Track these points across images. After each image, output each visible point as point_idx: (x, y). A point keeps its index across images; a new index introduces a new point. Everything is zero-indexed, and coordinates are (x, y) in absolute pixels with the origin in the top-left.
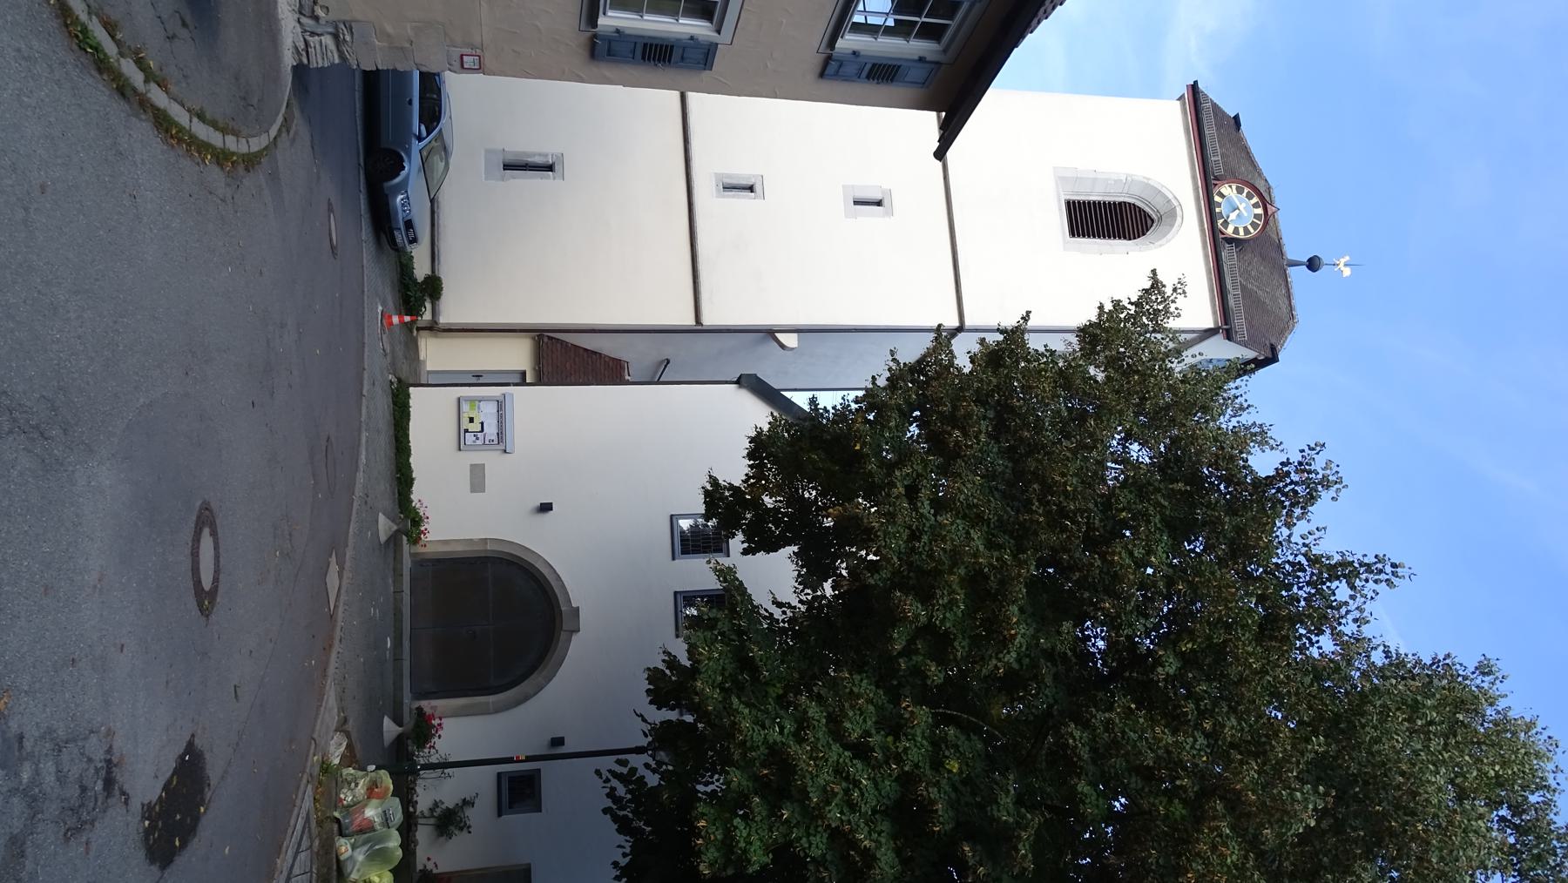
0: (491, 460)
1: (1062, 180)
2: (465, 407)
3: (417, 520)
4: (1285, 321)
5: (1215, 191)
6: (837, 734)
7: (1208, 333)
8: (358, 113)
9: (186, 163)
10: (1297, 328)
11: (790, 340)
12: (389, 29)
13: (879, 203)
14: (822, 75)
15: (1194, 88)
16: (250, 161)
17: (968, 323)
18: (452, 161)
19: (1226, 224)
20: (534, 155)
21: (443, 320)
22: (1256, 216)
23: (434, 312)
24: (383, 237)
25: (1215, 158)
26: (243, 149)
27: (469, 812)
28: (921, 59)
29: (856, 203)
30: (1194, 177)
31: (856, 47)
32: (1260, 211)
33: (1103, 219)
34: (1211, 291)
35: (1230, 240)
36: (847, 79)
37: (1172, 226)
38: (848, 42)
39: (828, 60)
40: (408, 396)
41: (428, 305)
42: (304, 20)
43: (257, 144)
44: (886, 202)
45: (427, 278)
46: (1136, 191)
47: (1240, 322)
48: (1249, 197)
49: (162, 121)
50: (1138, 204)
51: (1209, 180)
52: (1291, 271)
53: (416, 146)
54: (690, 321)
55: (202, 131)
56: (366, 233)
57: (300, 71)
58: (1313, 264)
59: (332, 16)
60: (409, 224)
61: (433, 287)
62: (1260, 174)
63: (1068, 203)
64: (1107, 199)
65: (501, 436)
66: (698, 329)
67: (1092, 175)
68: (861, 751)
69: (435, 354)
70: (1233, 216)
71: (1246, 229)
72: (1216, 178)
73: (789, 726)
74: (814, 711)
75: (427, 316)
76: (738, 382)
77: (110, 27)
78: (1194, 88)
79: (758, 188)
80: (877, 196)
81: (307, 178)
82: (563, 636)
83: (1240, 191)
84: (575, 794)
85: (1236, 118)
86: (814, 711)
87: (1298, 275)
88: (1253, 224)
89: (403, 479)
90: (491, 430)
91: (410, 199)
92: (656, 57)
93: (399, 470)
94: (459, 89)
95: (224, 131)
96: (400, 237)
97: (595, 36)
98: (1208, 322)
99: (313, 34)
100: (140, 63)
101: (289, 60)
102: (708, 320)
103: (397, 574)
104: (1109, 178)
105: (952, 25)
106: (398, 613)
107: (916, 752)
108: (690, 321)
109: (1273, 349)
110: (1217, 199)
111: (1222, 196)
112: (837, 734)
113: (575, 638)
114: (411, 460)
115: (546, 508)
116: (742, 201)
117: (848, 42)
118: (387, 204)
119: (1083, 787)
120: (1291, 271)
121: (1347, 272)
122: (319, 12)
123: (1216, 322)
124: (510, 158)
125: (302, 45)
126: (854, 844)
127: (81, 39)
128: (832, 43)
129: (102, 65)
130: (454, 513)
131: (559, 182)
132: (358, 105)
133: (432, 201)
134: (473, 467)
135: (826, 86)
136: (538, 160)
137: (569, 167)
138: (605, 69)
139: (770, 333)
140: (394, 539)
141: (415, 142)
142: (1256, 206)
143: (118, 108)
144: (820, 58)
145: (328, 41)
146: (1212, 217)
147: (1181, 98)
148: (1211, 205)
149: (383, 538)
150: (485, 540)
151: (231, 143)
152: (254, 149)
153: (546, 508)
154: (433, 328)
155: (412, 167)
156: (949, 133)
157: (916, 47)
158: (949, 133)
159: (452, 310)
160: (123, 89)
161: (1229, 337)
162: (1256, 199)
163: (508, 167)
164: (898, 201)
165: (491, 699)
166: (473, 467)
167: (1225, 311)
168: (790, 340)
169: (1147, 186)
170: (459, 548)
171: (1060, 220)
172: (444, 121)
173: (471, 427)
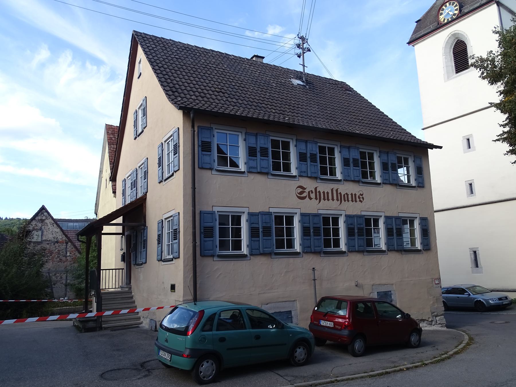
1: (449, 78)
5: (443, 23)
8: (469, 313)
9: (468, 351)
12: (432, 302)
13: (468, 140)
14: (423, 187)
15: (409, 43)
16: (471, 339)
18: (476, 285)
19: (454, 15)
20: (471, 258)
22: (450, 5)
24: (508, 307)
25: (432, 27)
26: (467, 340)
28: (414, 161)
29: (470, 148)
30: (439, 32)
31: (414, 180)
32: (448, 4)
34: (481, 10)
35: (460, 11)
36: (423, 180)
37: (458, 33)
38: (413, 183)
39: (419, 187)
42: (433, 324)
43: (466, 337)
44: (468, 138)
48: (443, 10)
49: (456, 353)
50: (453, 48)
51: (440, 26)
53: (472, 296)
55: (460, 347)
56: (504, 313)
57: (447, 327)
59: (431, 317)
60: (500, 299)
62: (435, 4)
64: (453, 59)
70: (451, 13)
71: (455, 7)
72: (438, 24)
77: (435, 358)
79: (470, 182)
80: (466, 141)
81: (480, 328)
83: (442, 14)
85: (416, 22)
88: (453, 5)
91: (492, 298)
92: (427, 232)
94: (447, 282)
95: (461, 343)
96: (505, 302)
97: (424, 250)
99: (436, 322)
100: (442, 355)
101: (445, 329)
105: (403, 156)
110: (446, 21)
111: (445, 19)
116: (475, 187)
117: (413, 183)
118: (493, 306)
122: (430, 320)
123: (494, 4)
124: (474, 265)
125: (440, 325)
127: (438, 362)
128: (414, 187)
129: (443, 360)
131: (479, 249)
132: (462, 313)
133: (491, 291)
135: (426, 185)
136: (473, 256)
137: (474, 246)
138: (433, 245)
141: (471, 296)
142: (446, 6)
143: (452, 359)
144: (418, 189)
145: (438, 318)
146: (453, 20)
148: (449, 23)
151: (465, 342)
152: (468, 338)
155: (479, 297)
156: (432, 147)
157: (411, 164)
158: (432, 147)
160: (449, 358)
162: (444, 7)
163: (477, 266)
164: (466, 134)
169: (446, 47)
172: (462, 287)
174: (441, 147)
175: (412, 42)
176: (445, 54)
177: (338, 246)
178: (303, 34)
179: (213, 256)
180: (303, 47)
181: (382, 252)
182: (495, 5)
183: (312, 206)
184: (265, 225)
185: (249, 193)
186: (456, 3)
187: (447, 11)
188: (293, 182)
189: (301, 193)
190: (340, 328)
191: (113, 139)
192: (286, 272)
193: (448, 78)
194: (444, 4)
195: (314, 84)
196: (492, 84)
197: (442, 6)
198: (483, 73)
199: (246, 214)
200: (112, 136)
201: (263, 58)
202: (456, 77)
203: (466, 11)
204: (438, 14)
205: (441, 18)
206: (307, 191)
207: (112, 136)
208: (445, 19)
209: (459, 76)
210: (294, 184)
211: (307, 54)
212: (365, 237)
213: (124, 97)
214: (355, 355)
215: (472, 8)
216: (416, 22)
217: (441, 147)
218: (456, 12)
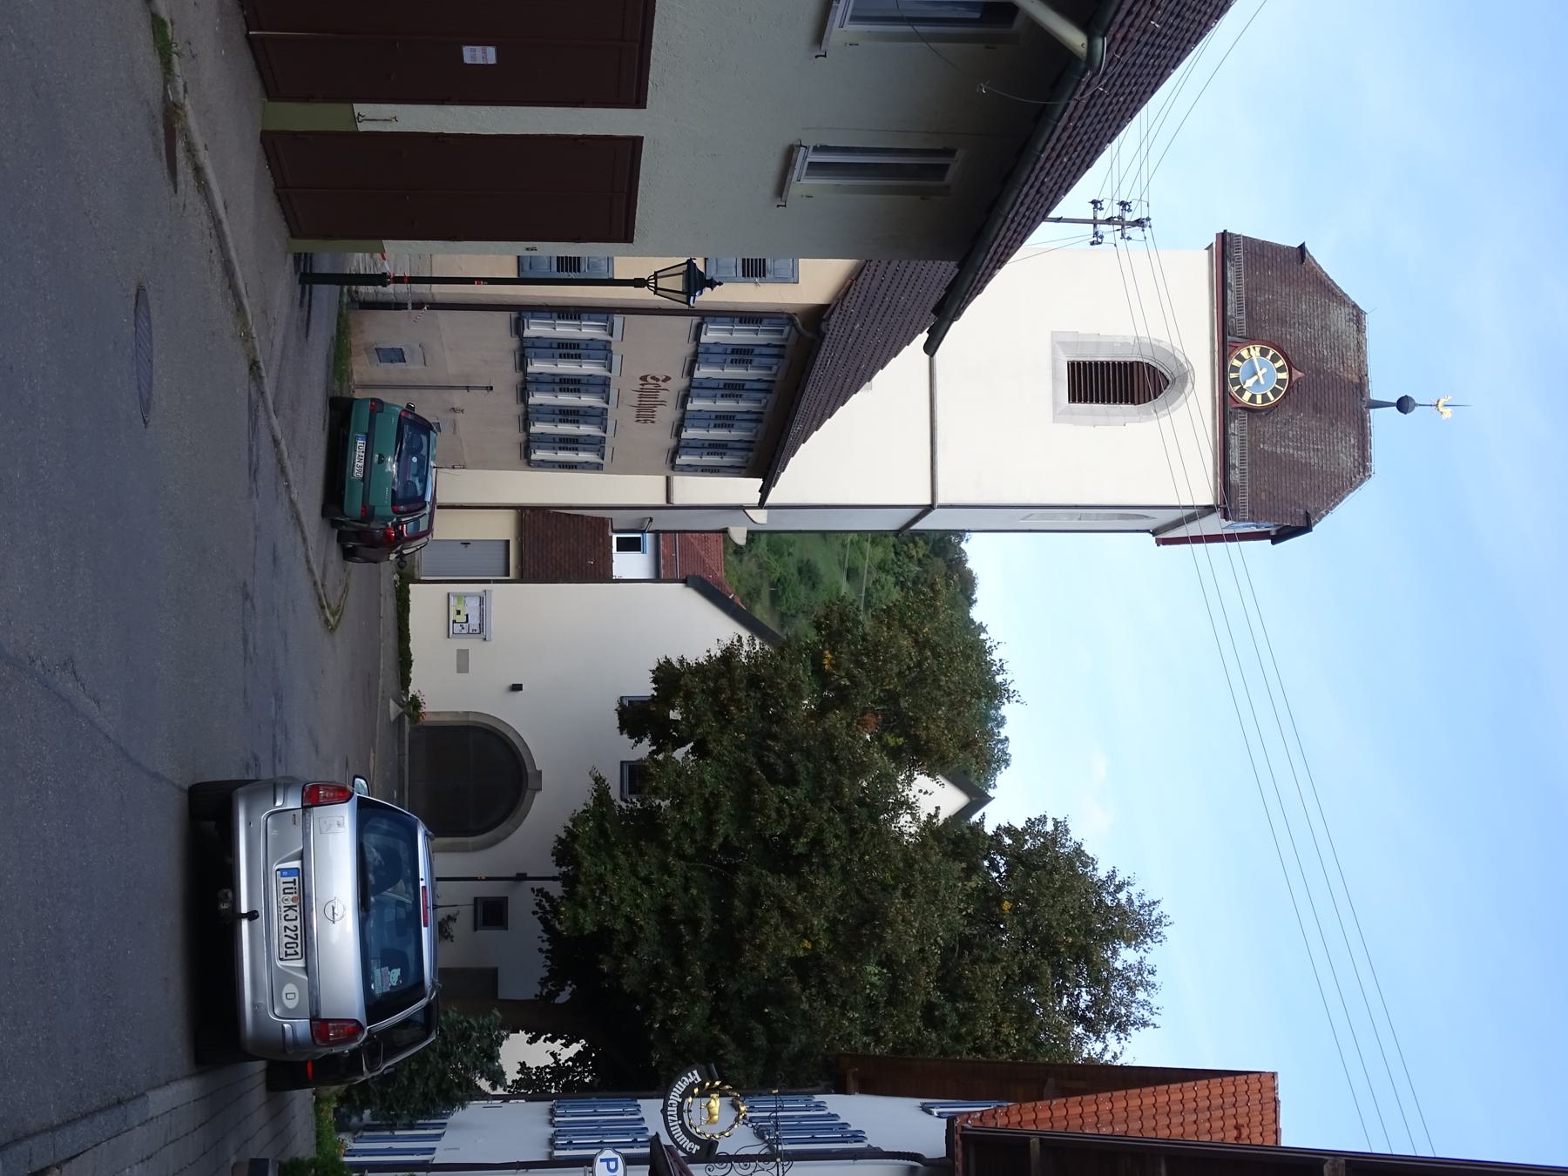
1: (1058, 342)
3: (415, 703)
6: (635, 873)
7: (1209, 510)
10: (1367, 486)
17: (941, 500)
19: (1241, 391)
27: (452, 925)
30: (1212, 339)
33: (1110, 382)
37: (1182, 391)
46: (1147, 352)
47: (1243, 500)
51: (1227, 342)
52: (1374, 413)
54: (662, 501)
58: (1404, 405)
65: (481, 625)
67: (1094, 339)
68: (647, 881)
70: (1249, 383)
73: (609, 867)
74: (622, 859)
76: (684, 581)
82: (528, 793)
83: (1264, 353)
84: (522, 904)
85: (1302, 247)
86: (622, 859)
87: (1382, 422)
89: (404, 661)
90: (474, 622)
98: (1208, 500)
102: (677, 501)
103: (401, 741)
104: (1115, 333)
106: (401, 770)
107: (674, 883)
108: (662, 501)
109: (1307, 517)
111: (1241, 359)
112: (635, 873)
113: (538, 796)
119: (737, 903)
120: (1374, 413)
126: (635, 923)
130: (440, 687)
140: (400, 718)
142: (1280, 370)
147: (1209, 248)
149: (393, 718)
150: (467, 713)
153: (517, 688)
161: (1226, 517)
165: (470, 840)
167: (1225, 485)
170: (448, 718)
173: (459, 619)
182: (1210, 502)
187: (1260, 374)
193: (1062, 344)
203: (1233, 427)
208: (1241, 359)
209: (1055, 378)
215: (1234, 441)
216: (1302, 247)
218: (1246, 397)
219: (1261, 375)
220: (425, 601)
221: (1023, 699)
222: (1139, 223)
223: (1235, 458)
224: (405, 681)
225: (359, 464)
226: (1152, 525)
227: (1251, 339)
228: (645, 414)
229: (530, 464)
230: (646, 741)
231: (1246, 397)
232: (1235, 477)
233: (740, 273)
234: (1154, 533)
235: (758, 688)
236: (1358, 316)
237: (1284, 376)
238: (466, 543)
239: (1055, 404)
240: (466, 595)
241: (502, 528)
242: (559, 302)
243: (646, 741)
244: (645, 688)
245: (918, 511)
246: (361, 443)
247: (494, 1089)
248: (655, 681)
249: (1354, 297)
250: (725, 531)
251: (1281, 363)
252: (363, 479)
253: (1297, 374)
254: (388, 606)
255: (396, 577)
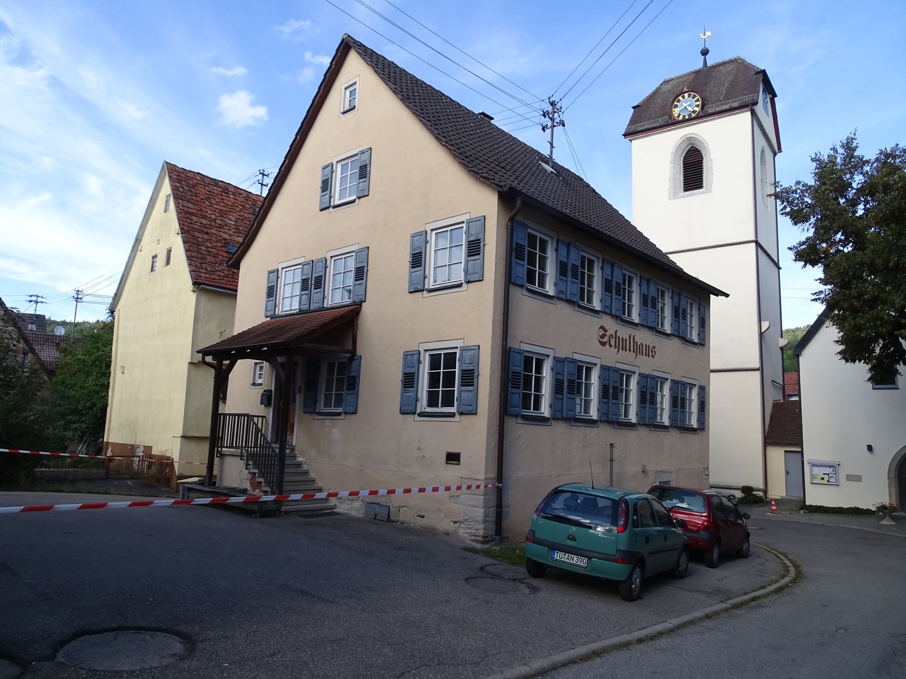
0: (842, 473)
1: (674, 196)
2: (816, 481)
3: (883, 508)
4: (739, 65)
7: (753, 114)
10: (743, 56)
11: (765, 325)
17: (753, 238)
19: (694, 112)
21: (762, 487)
22: (689, 96)
23: (759, 490)
25: (661, 122)
32: (686, 95)
33: (693, 170)
35: (703, 108)
40: (811, 506)
41: (755, 493)
45: (743, 492)
47: (747, 99)
51: (672, 123)
52: (709, 64)
58: (705, 53)
61: (747, 490)
62: (659, 89)
63: (685, 190)
65: (830, 467)
66: (761, 369)
69: (778, 491)
70: (690, 109)
75: (761, 494)
76: (798, 356)
78: (625, 135)
83: (676, 106)
85: (634, 108)
87: (711, 60)
88: (693, 98)
89: (855, 512)
90: (828, 470)
93: (851, 513)
98: (749, 114)
102: (758, 365)
108: (758, 373)
109: (758, 73)
111: (679, 115)
114: (845, 507)
115: (870, 448)
120: (709, 64)
121: (708, 33)
130: (874, 491)
134: (848, 479)
139: (761, 335)
140: (893, 518)
142: (684, 97)
146: (691, 119)
147: (631, 141)
148: (684, 121)
149: (894, 523)
150: (889, 478)
153: (870, 448)
154: (765, 491)
156: (718, 293)
158: (718, 293)
159: (757, 482)
161: (756, 103)
162: (680, 98)
166: (848, 479)
168: (765, 325)
170: (893, 489)
171: (695, 196)
174: (727, 295)
175: (630, 134)
176: (673, 162)
177: (537, 407)
178: (555, 98)
179: (517, 416)
180: (552, 116)
181: (665, 428)
182: (749, 113)
183: (612, 357)
184: (465, 367)
185: (562, 331)
186: (698, 97)
187: (685, 105)
188: (596, 319)
189: (603, 336)
190: (695, 529)
191: (181, 189)
192: (584, 446)
193: (674, 195)
194: (682, 93)
195: (563, 174)
196: (796, 224)
197: (678, 96)
198: (785, 207)
199: (551, 358)
200: (177, 184)
201: (492, 119)
202: (682, 197)
203: (711, 111)
204: (673, 105)
205: (676, 111)
206: (608, 334)
207: (177, 184)
208: (679, 115)
209: (690, 195)
210: (596, 322)
211: (558, 130)
212: (521, 391)
213: (297, 135)
214: (712, 565)
215: (718, 109)
216: (634, 108)
217: (727, 295)
218: (697, 109)
219: (687, 105)
220: (815, 496)
221: (853, 131)
222: (553, 104)
223: (727, 107)
224: (868, 512)
225: (575, 560)
226: (768, 153)
227: (671, 115)
228: (650, 352)
229: (703, 426)
230: (898, 367)
231: (697, 109)
232: (736, 105)
233: (477, 257)
234: (775, 154)
235: (849, 283)
236: (666, 82)
237: (686, 95)
238: (787, 473)
239: (703, 193)
240: (812, 474)
241: (777, 455)
242: (497, 386)
243: (898, 367)
244: (861, 369)
245: (759, 250)
246: (558, 556)
247: (254, 490)
248: (854, 361)
249: (658, 85)
250: (782, 349)
251: (680, 98)
252: (589, 558)
253: (685, 89)
254: (818, 518)
255: (802, 512)
